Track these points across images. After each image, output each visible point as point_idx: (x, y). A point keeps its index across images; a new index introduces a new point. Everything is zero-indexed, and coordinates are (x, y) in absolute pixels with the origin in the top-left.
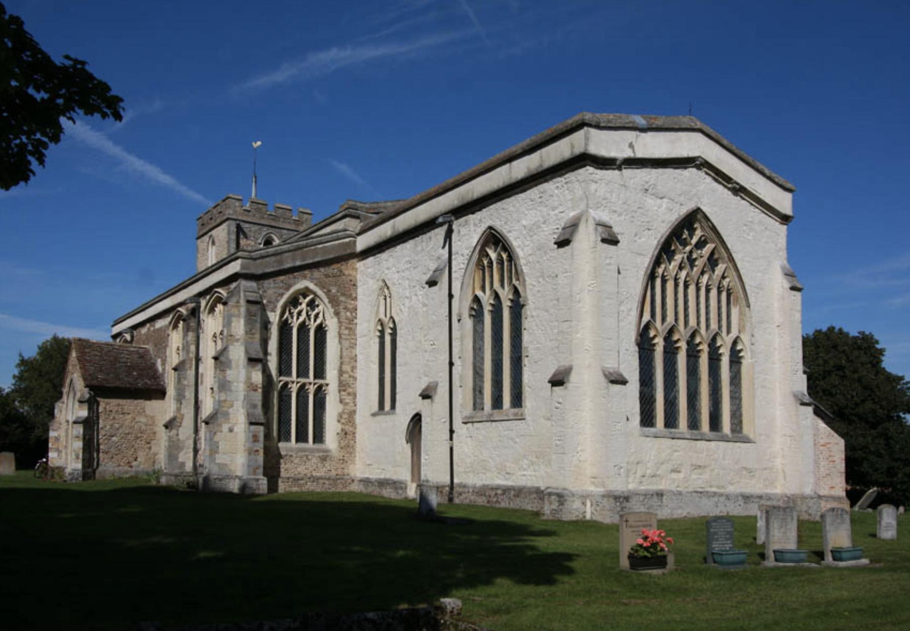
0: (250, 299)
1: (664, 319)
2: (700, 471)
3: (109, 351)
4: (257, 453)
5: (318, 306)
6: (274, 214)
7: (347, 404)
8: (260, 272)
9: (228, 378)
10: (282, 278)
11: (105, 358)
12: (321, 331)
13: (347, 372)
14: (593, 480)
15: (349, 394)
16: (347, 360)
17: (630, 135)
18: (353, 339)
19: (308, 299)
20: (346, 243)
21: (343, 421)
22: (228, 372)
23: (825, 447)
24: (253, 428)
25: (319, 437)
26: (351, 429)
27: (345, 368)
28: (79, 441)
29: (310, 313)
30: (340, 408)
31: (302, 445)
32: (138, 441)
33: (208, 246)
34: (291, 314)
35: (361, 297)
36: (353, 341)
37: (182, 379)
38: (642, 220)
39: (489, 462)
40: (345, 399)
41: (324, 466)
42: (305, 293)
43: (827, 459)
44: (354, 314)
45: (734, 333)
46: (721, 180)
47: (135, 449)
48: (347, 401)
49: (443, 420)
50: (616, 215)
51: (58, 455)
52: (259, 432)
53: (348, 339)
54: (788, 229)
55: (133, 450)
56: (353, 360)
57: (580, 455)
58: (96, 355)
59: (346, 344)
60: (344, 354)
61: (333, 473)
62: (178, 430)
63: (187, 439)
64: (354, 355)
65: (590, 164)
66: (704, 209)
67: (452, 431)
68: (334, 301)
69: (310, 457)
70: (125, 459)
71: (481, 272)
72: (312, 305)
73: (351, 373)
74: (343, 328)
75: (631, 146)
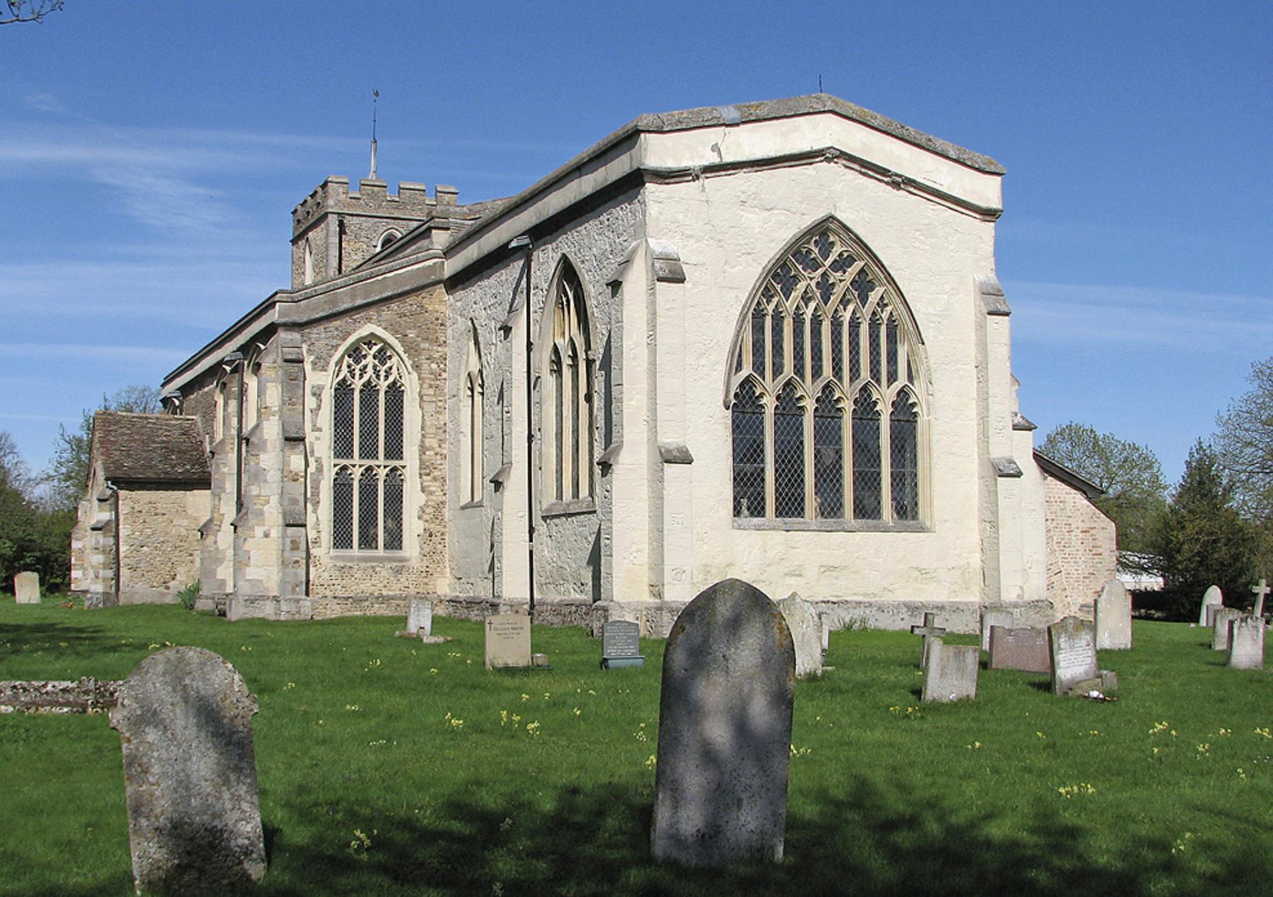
0: (289, 357)
1: (778, 370)
2: (834, 574)
3: (143, 427)
4: (296, 565)
5: (390, 357)
6: (397, 199)
7: (431, 493)
8: (305, 319)
9: (262, 465)
10: (337, 323)
11: (136, 437)
12: (395, 392)
13: (432, 449)
14: (652, 588)
15: (435, 479)
16: (433, 430)
17: (714, 134)
18: (440, 401)
19: (375, 348)
20: (429, 266)
21: (426, 517)
22: (262, 457)
23: (1088, 534)
24: (290, 530)
25: (395, 540)
26: (439, 528)
27: (428, 442)
28: (98, 553)
29: (378, 369)
30: (422, 499)
31: (369, 553)
32: (177, 553)
33: (304, 253)
34: (352, 372)
35: (451, 341)
36: (440, 404)
37: (221, 466)
38: (736, 242)
39: (566, 569)
40: (428, 486)
41: (398, 580)
42: (370, 340)
43: (1090, 551)
44: (442, 366)
45: (902, 380)
46: (871, 173)
47: (173, 563)
48: (433, 489)
49: (520, 514)
50: (693, 241)
51: (84, 575)
52: (300, 537)
53: (434, 402)
54: (996, 228)
55: (170, 564)
56: (440, 431)
57: (635, 557)
58: (124, 434)
59: (430, 408)
60: (428, 423)
61: (412, 591)
62: (216, 537)
63: (227, 549)
64: (442, 423)
65: (649, 180)
66: (839, 215)
67: (531, 530)
68: (411, 349)
69: (377, 569)
70: (159, 576)
71: (561, 311)
72: (382, 356)
73: (438, 450)
74: (425, 386)
75: (716, 148)
